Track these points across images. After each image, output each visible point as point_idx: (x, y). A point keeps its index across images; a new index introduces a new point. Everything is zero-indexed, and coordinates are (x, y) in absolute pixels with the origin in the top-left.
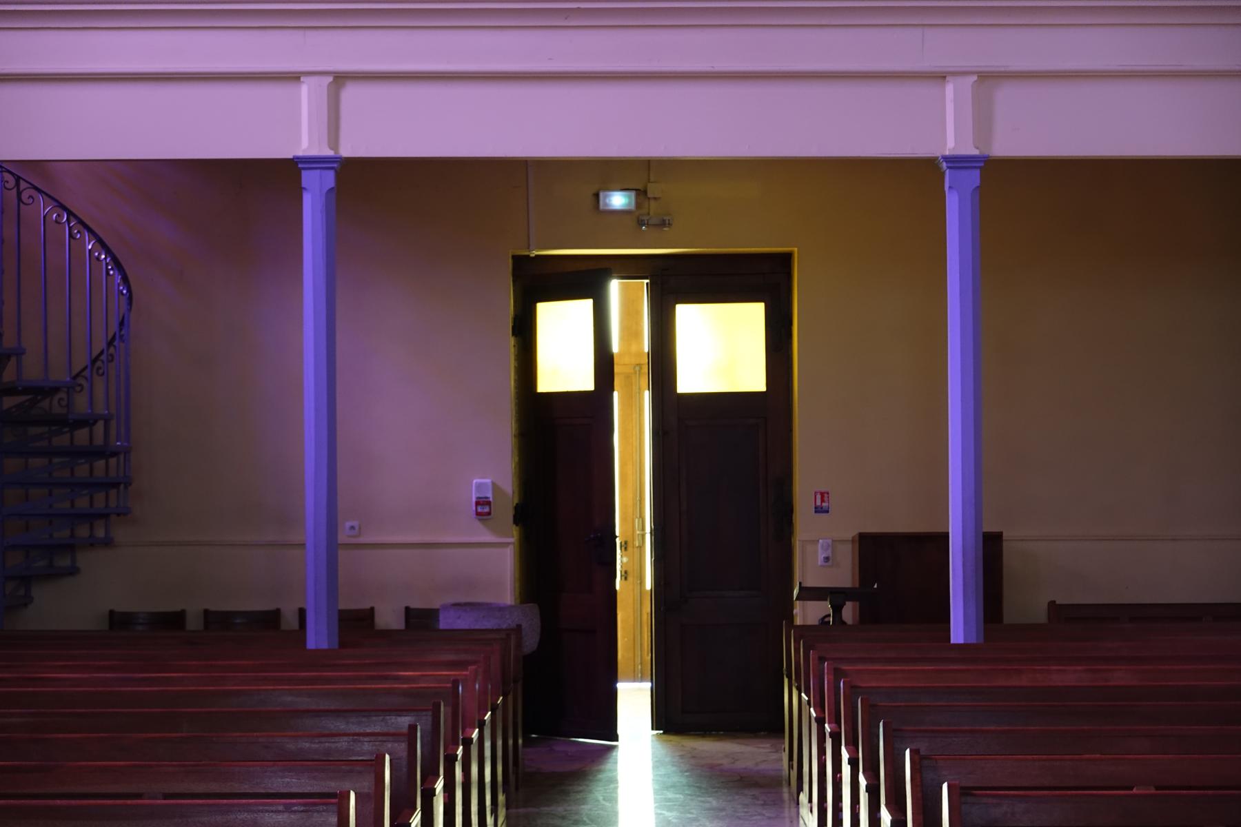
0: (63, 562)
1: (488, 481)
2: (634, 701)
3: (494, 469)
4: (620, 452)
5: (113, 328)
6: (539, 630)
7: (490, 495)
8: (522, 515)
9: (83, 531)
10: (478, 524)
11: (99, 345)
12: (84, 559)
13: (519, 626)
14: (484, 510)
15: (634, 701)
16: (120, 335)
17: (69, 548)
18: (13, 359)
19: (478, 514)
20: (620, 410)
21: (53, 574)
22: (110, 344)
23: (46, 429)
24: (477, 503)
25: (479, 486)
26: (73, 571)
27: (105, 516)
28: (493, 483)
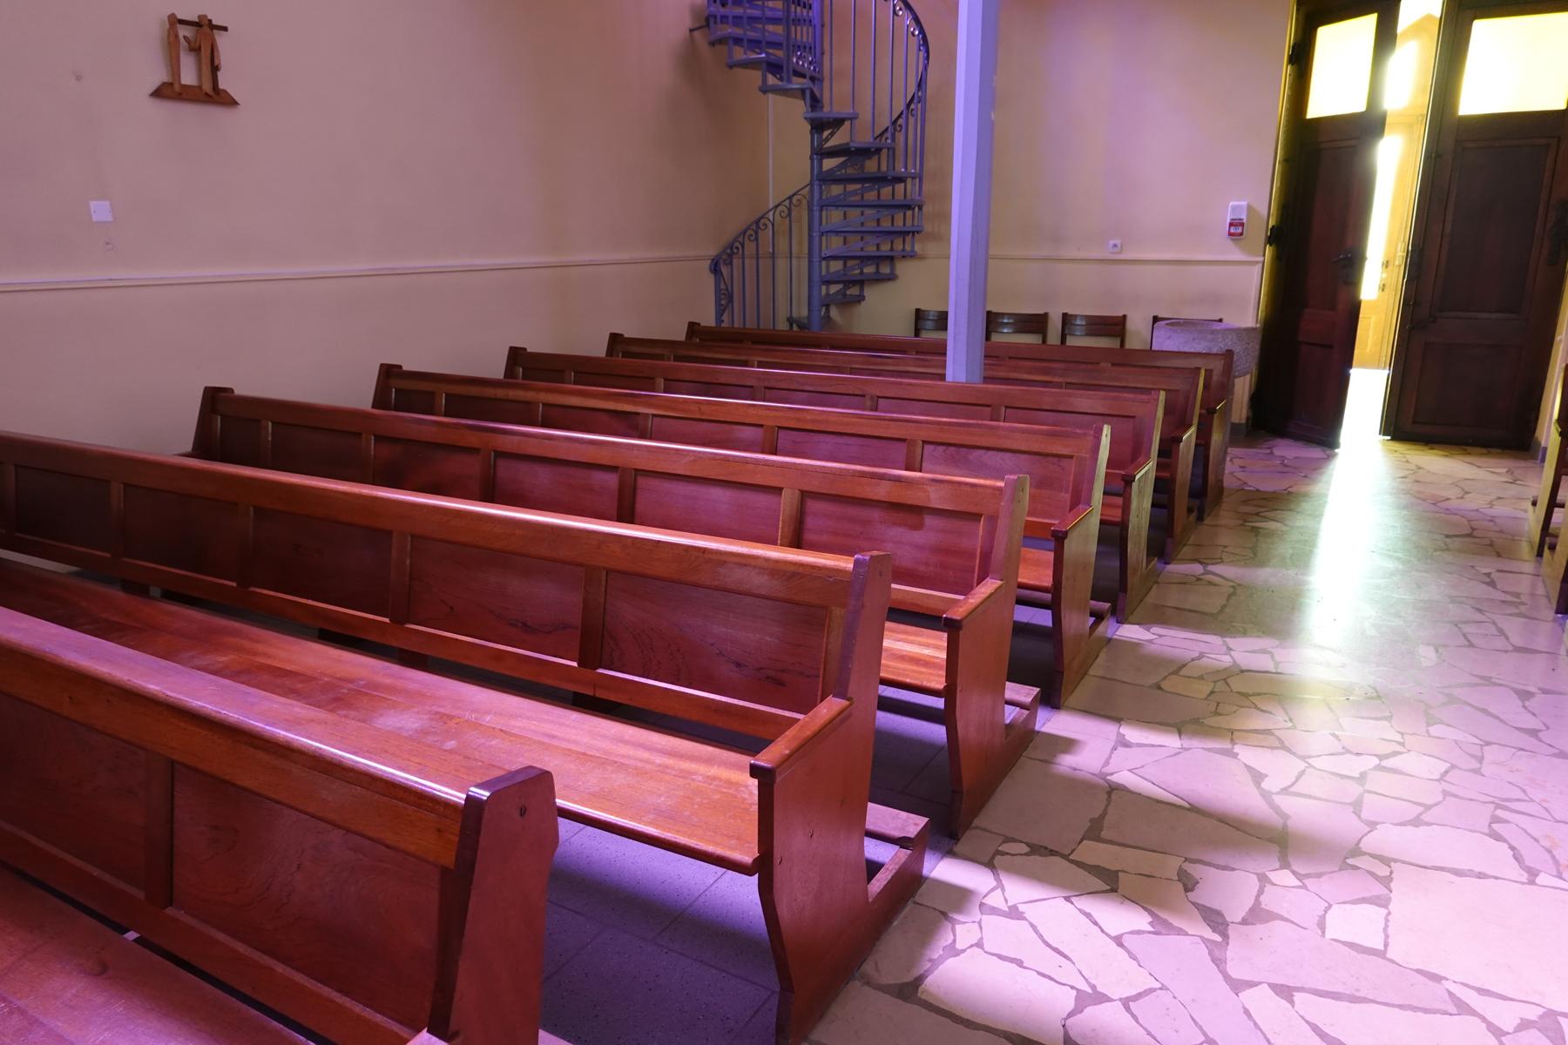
0: (885, 270)
1: (1244, 203)
2: (1367, 390)
3: (1254, 192)
4: (632, 819)
5: (912, 88)
6: (1257, 354)
7: (1244, 217)
8: (1276, 237)
9: (869, 270)
10: (1229, 243)
11: (900, 106)
12: (902, 268)
13: (1230, 353)
14: (1237, 229)
15: (1367, 390)
16: (917, 101)
17: (861, 283)
18: (847, 123)
19: (1230, 234)
20: (603, 810)
21: (879, 279)
22: (908, 105)
23: (858, 186)
24: (1231, 225)
25: (1234, 208)
26: (892, 277)
27: (891, 258)
28: (1249, 208)
